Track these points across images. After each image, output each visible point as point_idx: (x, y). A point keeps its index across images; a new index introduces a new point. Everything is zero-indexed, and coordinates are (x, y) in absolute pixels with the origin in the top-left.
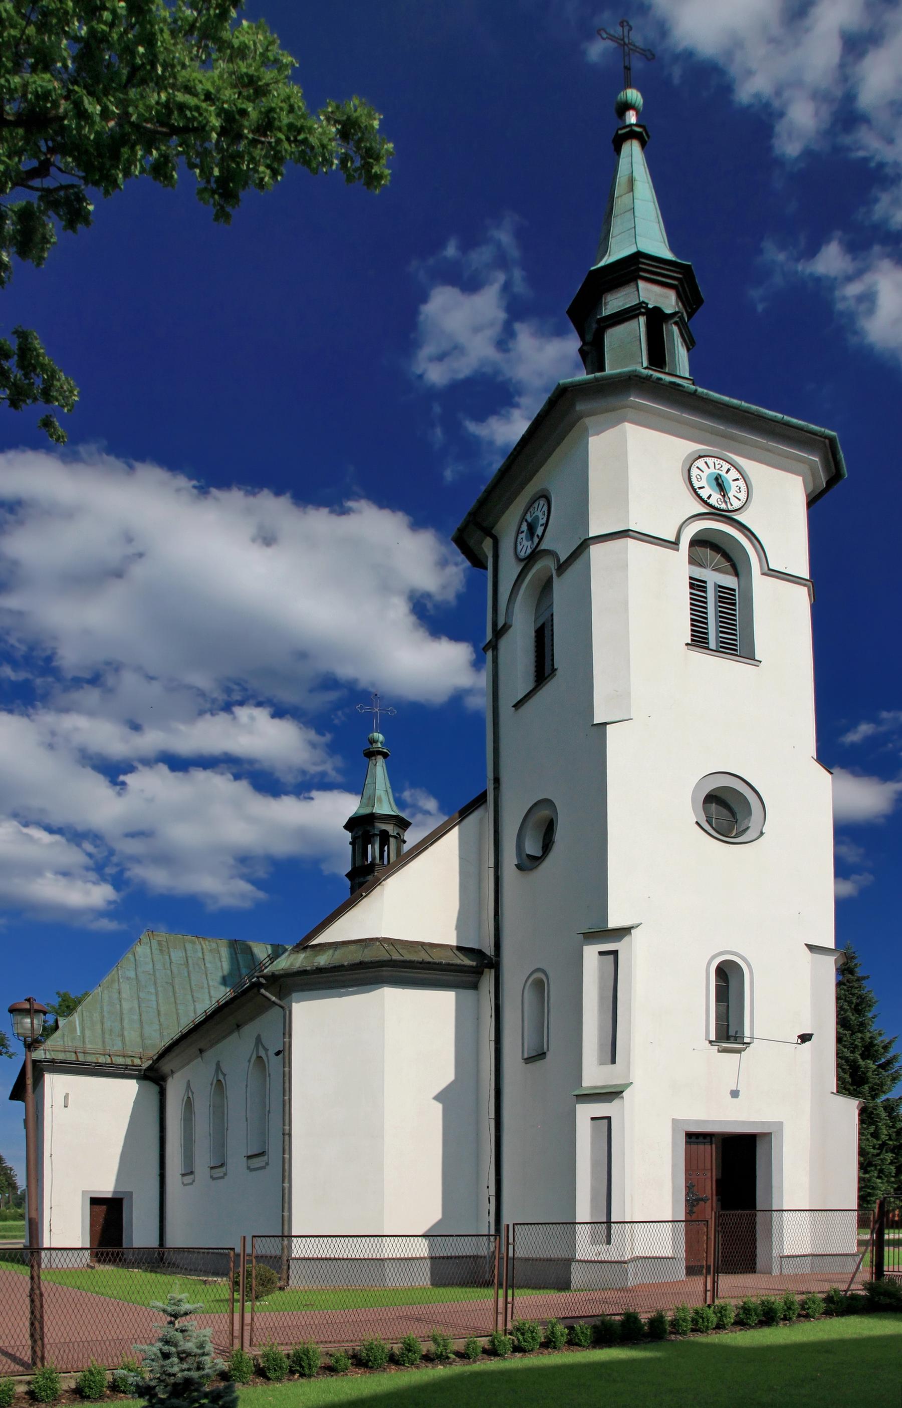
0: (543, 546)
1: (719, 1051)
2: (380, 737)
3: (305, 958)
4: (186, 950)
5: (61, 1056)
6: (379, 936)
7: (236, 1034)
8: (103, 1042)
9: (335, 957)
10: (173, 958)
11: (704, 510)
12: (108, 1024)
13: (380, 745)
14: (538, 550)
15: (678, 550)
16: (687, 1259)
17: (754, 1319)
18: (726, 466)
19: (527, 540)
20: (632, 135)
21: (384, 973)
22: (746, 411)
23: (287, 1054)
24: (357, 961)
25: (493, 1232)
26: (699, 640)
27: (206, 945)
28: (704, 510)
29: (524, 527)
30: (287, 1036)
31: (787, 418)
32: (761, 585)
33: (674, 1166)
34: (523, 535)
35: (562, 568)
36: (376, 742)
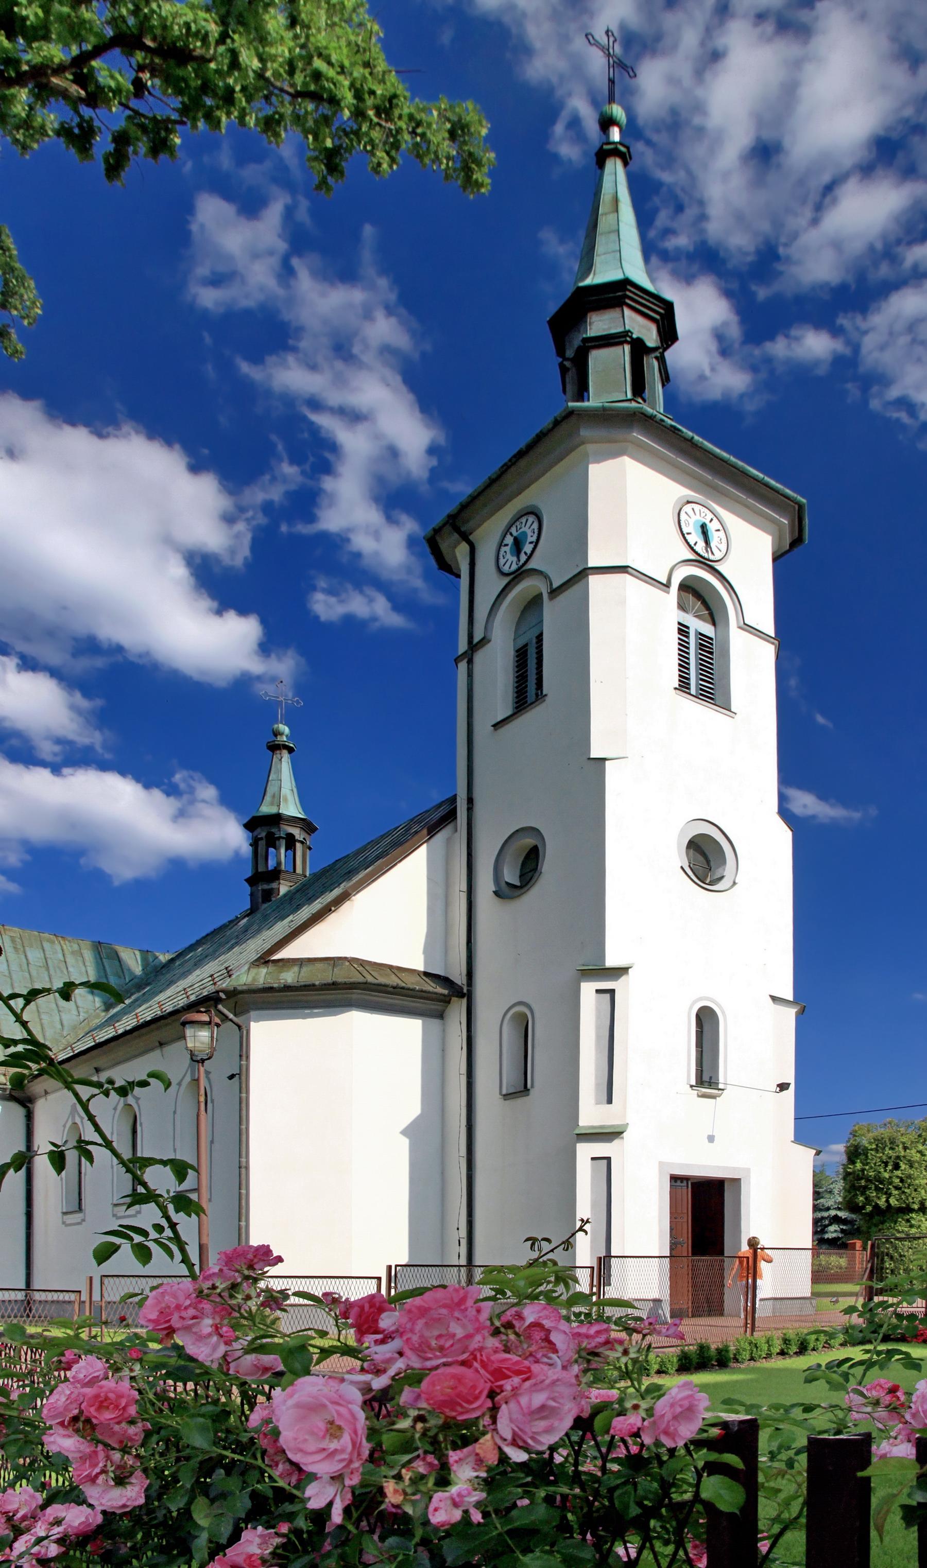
0: (532, 565)
1: (699, 1096)
2: (286, 730)
3: (267, 973)
4: (44, 950)
6: (348, 956)
9: (302, 974)
11: (692, 556)
14: (525, 568)
15: (668, 593)
17: (794, 1349)
18: (710, 516)
19: (512, 555)
20: (615, 153)
22: (734, 466)
23: (243, 1078)
24: (330, 981)
26: (684, 685)
27: (67, 946)
28: (692, 556)
29: (509, 540)
30: (244, 1058)
31: (767, 479)
32: (738, 641)
34: (507, 549)
35: (554, 592)
36: (282, 734)
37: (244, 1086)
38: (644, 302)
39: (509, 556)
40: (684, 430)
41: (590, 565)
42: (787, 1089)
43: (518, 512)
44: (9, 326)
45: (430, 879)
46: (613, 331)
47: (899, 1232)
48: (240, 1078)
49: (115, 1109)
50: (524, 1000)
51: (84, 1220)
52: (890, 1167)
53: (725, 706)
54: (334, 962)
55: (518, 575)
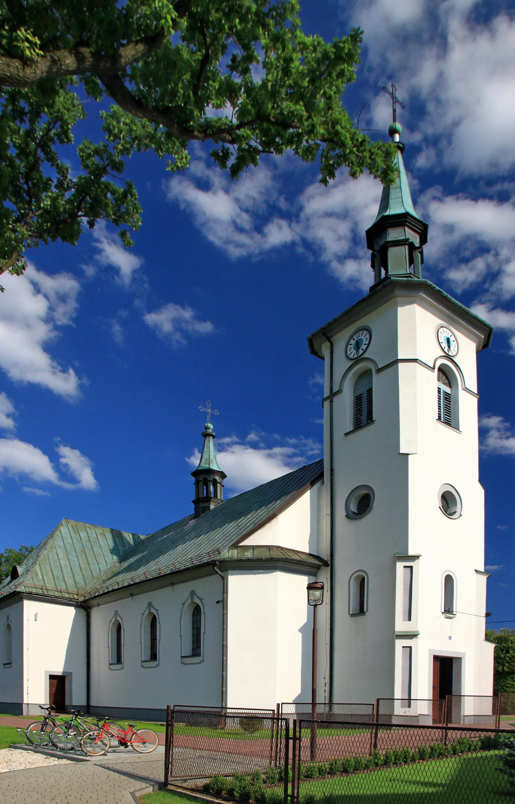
1: (445, 618)
2: (211, 426)
5: (34, 591)
6: (275, 545)
7: (170, 588)
8: (55, 584)
9: (255, 553)
10: (82, 537)
11: (443, 354)
12: (55, 573)
13: (211, 431)
14: (362, 357)
16: (433, 715)
18: (450, 334)
19: (354, 349)
21: (279, 565)
22: (460, 308)
23: (225, 603)
25: (327, 702)
26: (439, 419)
28: (443, 354)
29: (353, 342)
32: (462, 395)
33: (429, 671)
34: (352, 346)
35: (379, 371)
36: (209, 428)
37: (225, 607)
38: (414, 224)
39: (352, 350)
40: (444, 292)
41: (399, 358)
42: (490, 616)
43: (357, 329)
44: (126, 231)
45: (311, 508)
46: (400, 238)
47: (507, 683)
48: (223, 603)
49: (143, 614)
50: (363, 569)
51: (123, 668)
52: (504, 652)
53: (457, 428)
54: (269, 548)
55: (358, 360)
